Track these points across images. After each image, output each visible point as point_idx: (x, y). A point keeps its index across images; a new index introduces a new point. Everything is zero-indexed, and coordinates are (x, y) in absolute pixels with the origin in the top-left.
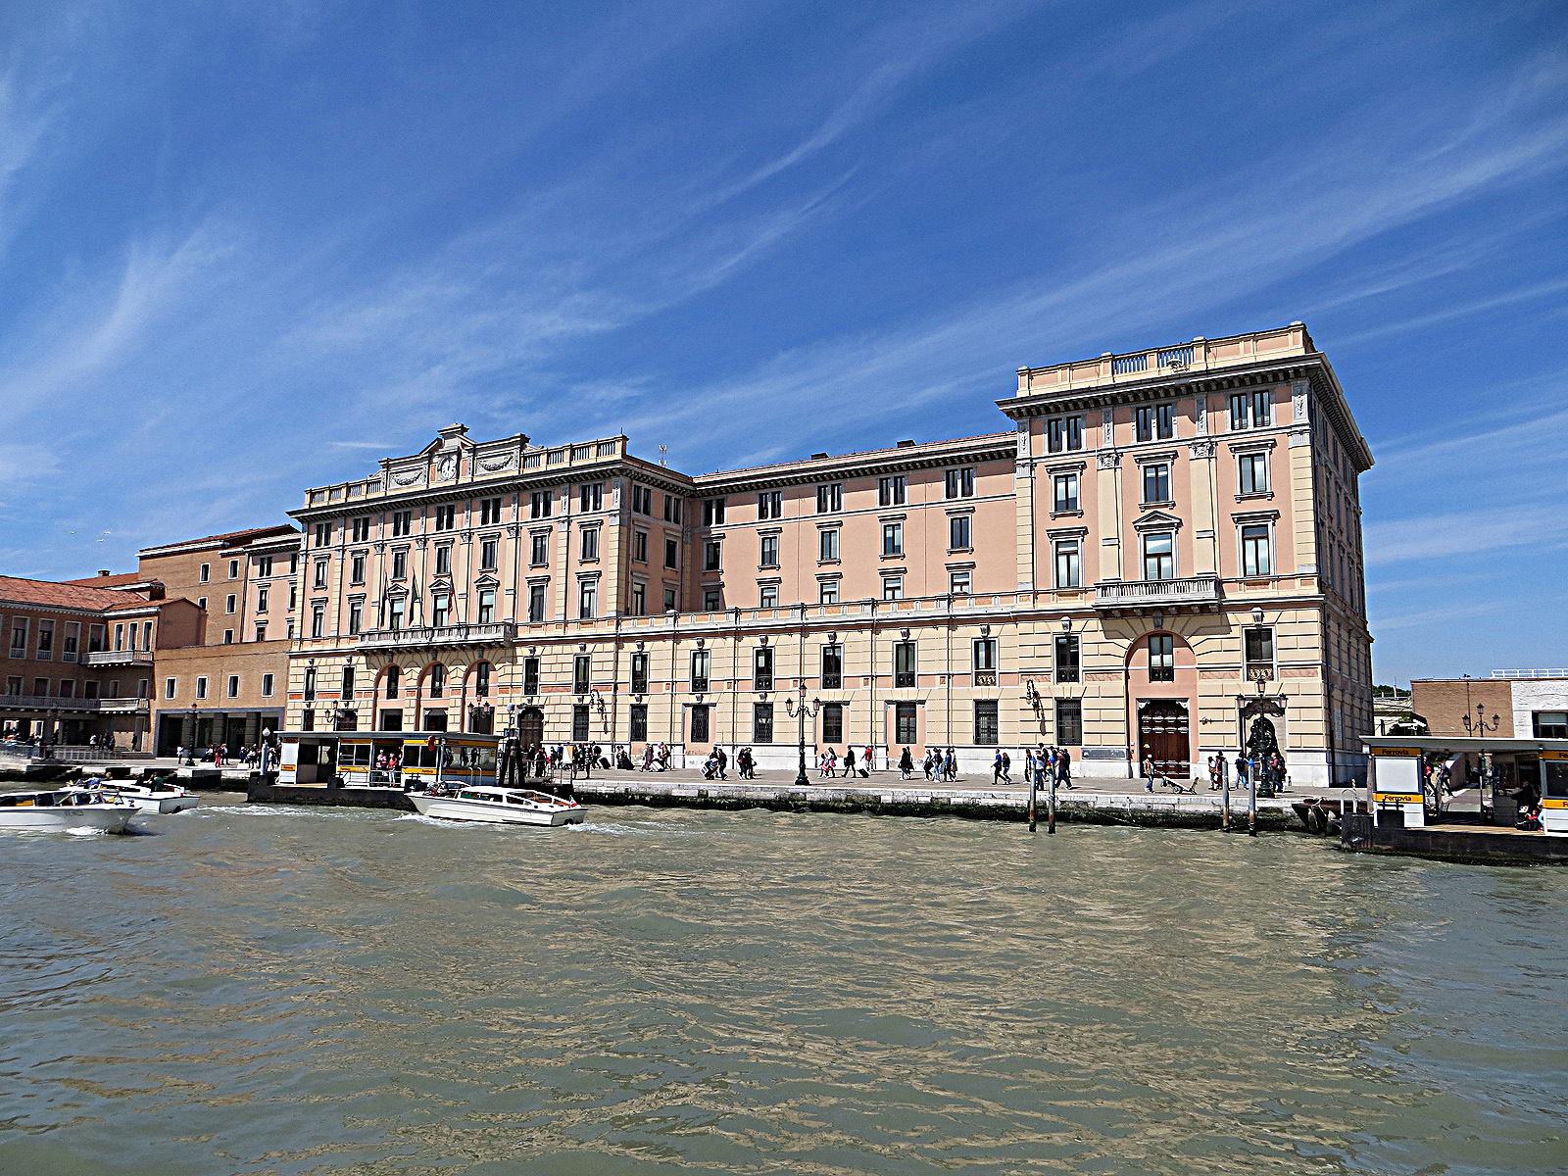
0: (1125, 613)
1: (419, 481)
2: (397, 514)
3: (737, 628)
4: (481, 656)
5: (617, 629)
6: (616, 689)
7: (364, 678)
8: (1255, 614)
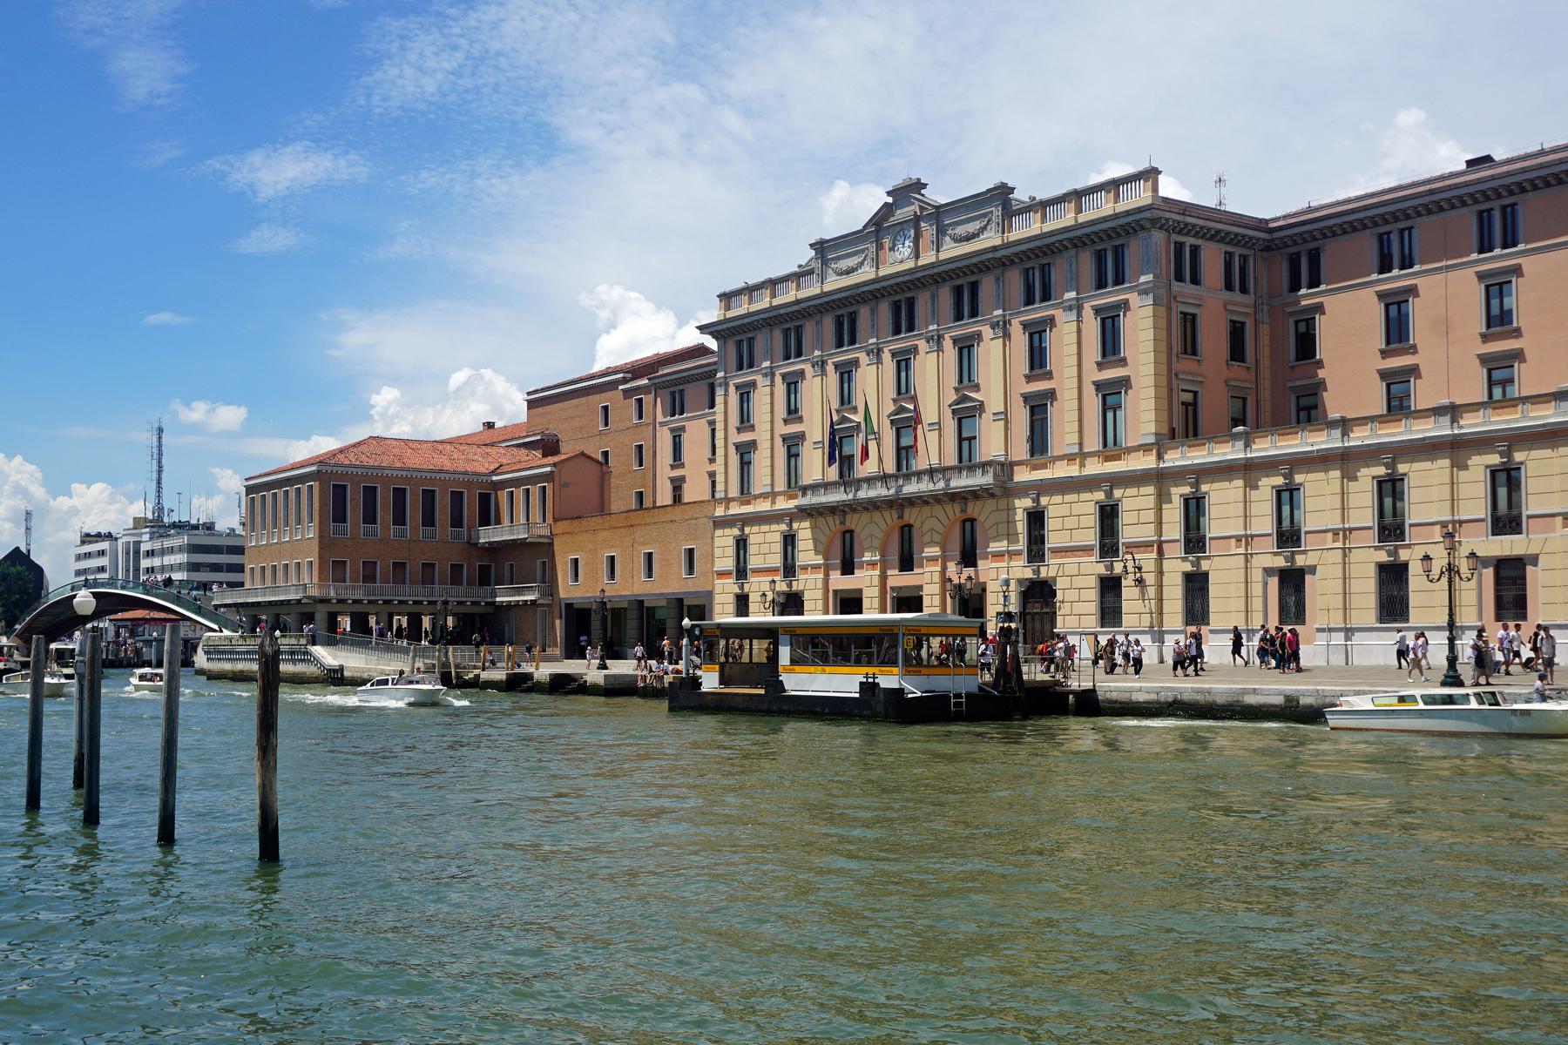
1: (866, 268)
4: (963, 511)
6: (1160, 552)
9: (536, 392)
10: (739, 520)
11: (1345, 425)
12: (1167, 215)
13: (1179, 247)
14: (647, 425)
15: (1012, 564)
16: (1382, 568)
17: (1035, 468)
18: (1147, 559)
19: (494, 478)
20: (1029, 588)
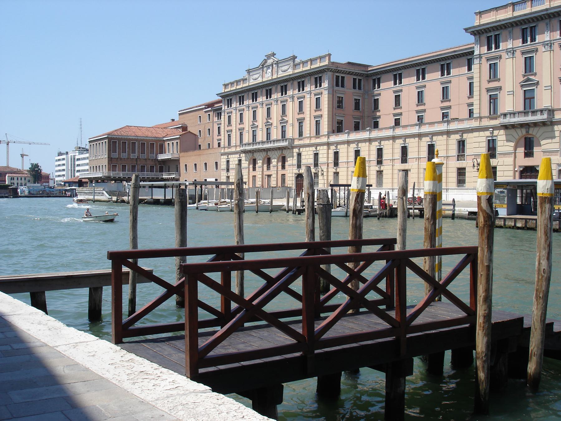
0: (514, 126)
2: (523, 30)
3: (448, 130)
5: (328, 140)
6: (328, 166)
7: (245, 164)
9: (181, 111)
10: (356, 141)
12: (332, 68)
13: (337, 77)
15: (293, 169)
16: (335, 173)
18: (324, 168)
19: (164, 139)
20: (524, 169)
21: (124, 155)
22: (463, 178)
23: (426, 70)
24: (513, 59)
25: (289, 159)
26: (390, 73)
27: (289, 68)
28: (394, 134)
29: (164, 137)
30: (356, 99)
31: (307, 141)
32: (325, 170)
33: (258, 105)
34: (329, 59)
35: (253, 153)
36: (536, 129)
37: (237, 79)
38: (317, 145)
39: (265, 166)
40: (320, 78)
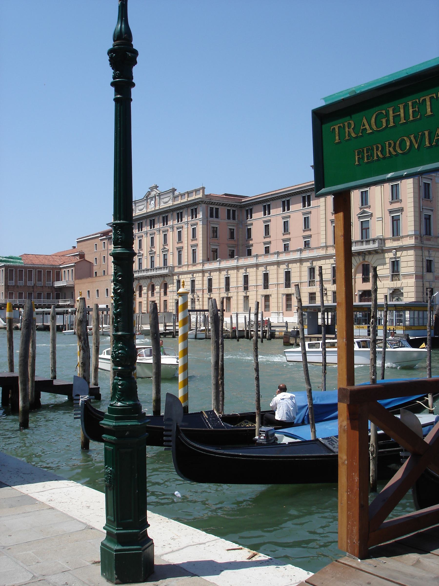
1: (170, 202)
3: (237, 265)
4: (364, 259)
5: (203, 267)
6: (203, 292)
8: (393, 253)
9: (79, 239)
11: (257, 256)
12: (205, 200)
13: (212, 209)
14: (106, 250)
16: (245, 297)
17: (394, 240)
18: (200, 294)
19: (61, 267)
20: (362, 293)
21: (21, 283)
22: (268, 303)
23: (271, 205)
24: (381, 187)
25: (170, 286)
26: (261, 204)
27: (169, 200)
28: (257, 262)
29: (60, 265)
30: (231, 229)
31: (185, 269)
32: (200, 296)
33: (169, 229)
34: (203, 192)
35: (139, 280)
36: (371, 257)
37: (189, 190)
38: (193, 272)
39: (150, 292)
40: (196, 209)
